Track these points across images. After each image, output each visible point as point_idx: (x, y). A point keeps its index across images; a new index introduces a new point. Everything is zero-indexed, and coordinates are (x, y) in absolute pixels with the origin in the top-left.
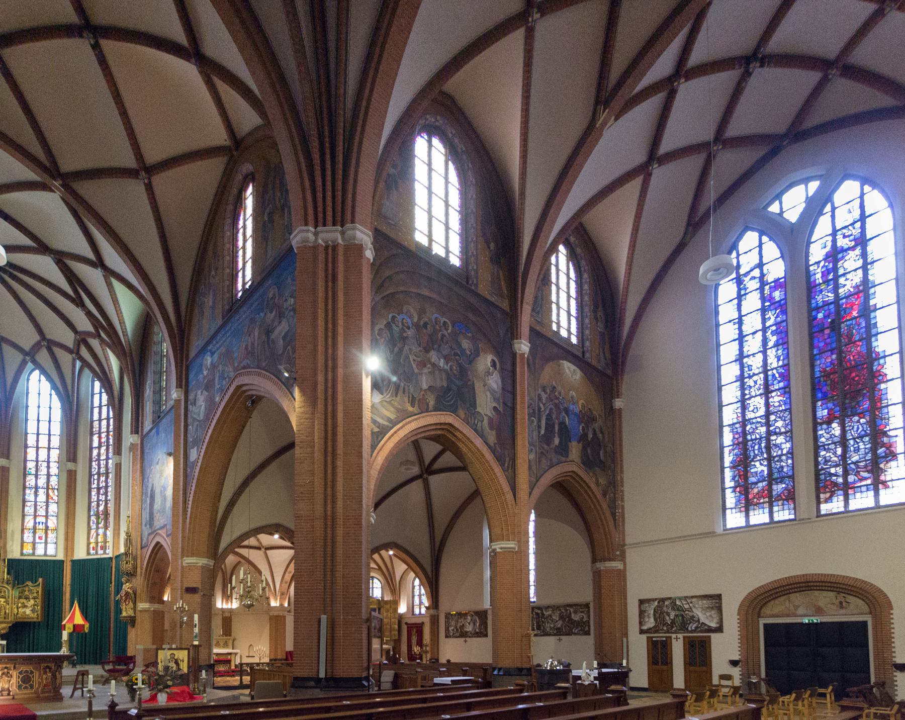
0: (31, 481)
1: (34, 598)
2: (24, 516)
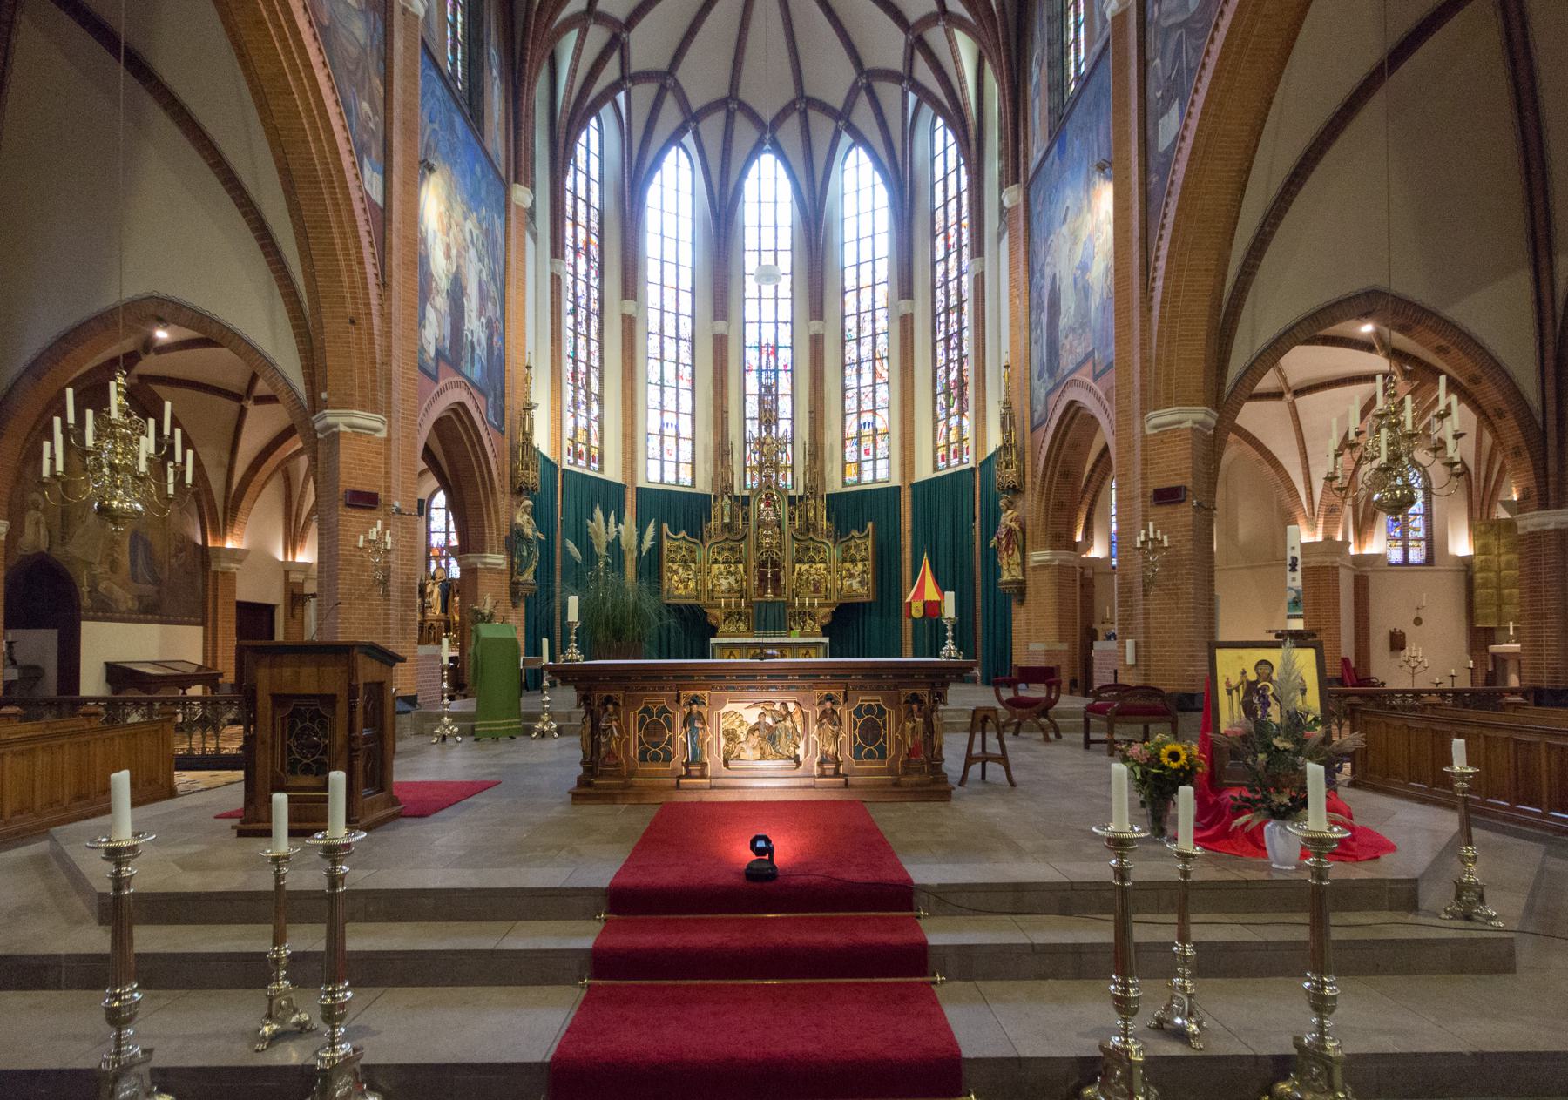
0: (851, 352)
1: (863, 560)
2: (844, 415)
